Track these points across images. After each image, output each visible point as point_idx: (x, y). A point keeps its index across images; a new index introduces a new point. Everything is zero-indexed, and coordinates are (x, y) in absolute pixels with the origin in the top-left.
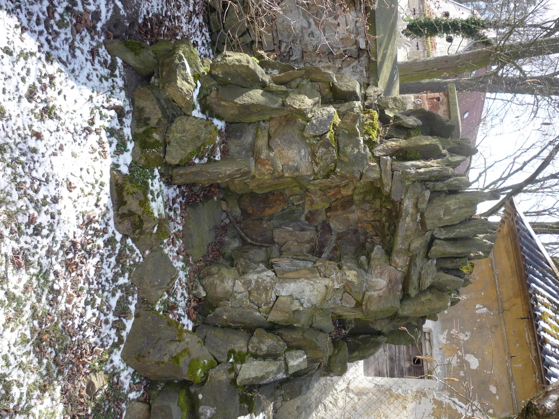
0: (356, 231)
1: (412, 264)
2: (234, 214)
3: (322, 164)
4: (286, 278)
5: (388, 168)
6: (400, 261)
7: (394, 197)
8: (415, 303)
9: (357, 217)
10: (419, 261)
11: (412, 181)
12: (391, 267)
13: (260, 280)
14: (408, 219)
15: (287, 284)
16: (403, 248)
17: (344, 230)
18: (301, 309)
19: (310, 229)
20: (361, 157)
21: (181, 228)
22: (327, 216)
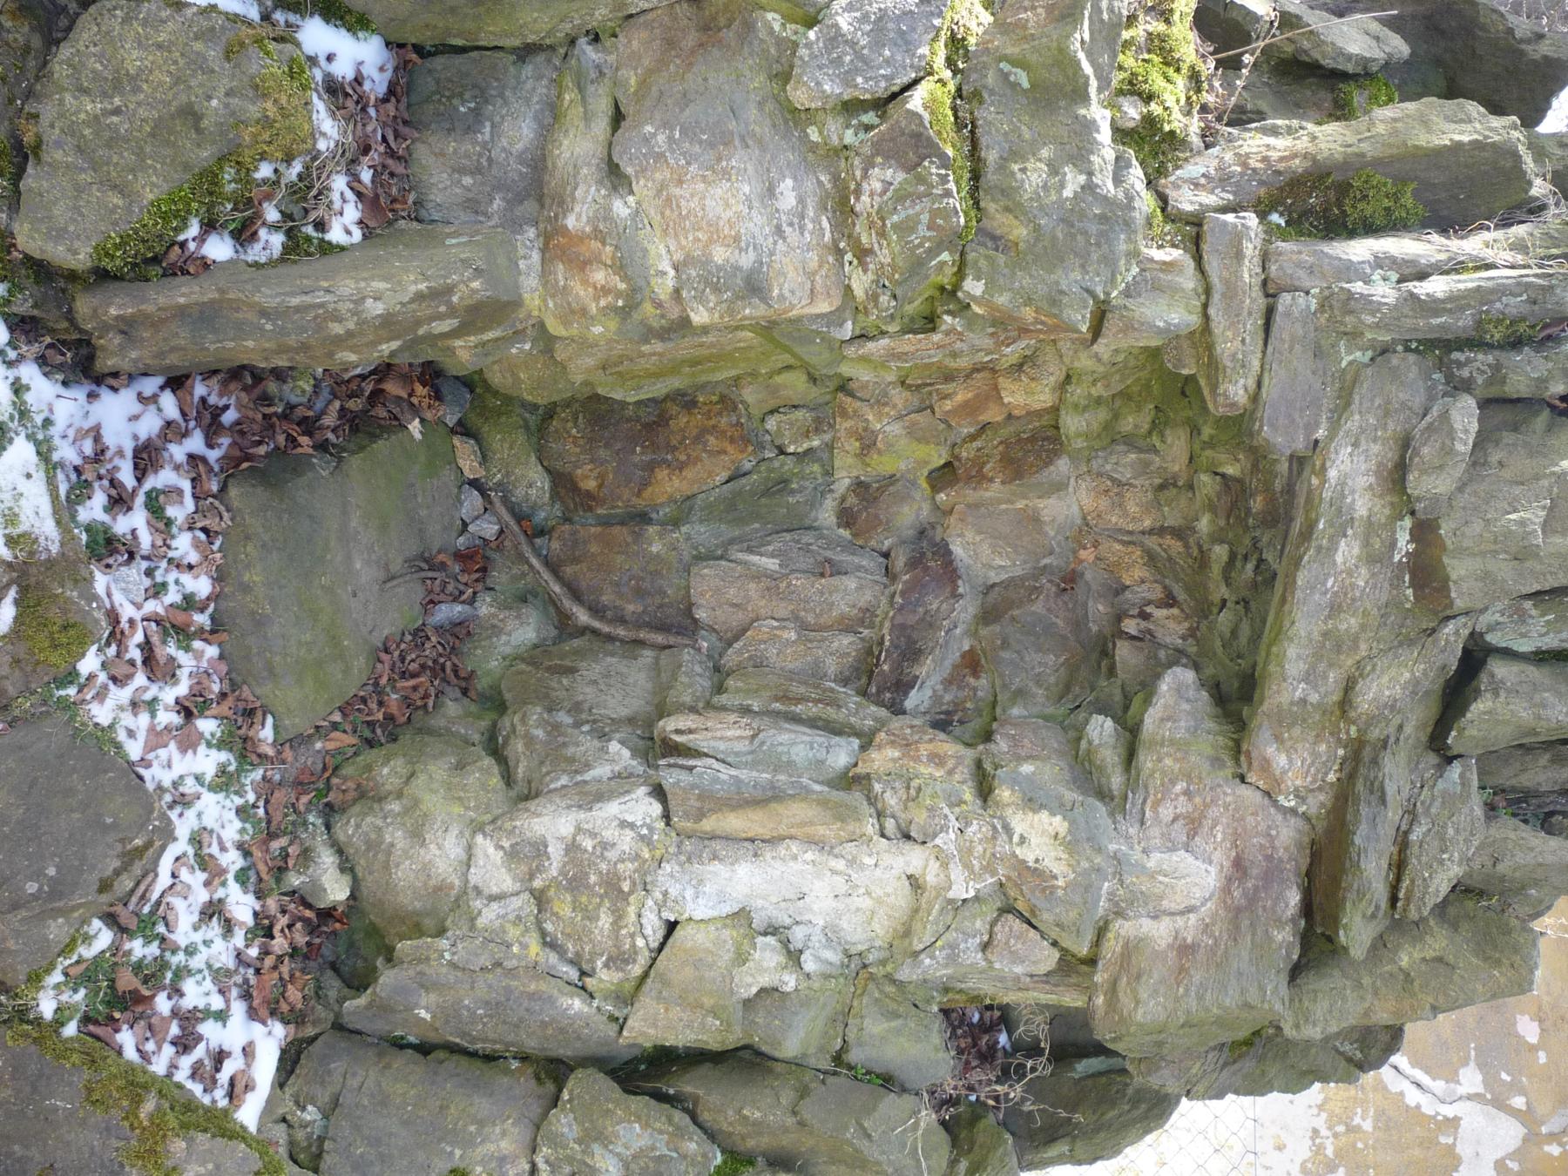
0: (1070, 580)
1: (1360, 786)
2: (519, 492)
3: (884, 256)
4: (713, 837)
5: (1249, 273)
6: (1296, 764)
7: (1280, 437)
8: (1366, 981)
9: (1075, 509)
10: (1396, 774)
11: (1372, 345)
12: (1244, 791)
13: (588, 844)
14: (1347, 552)
15: (716, 866)
16: (1314, 698)
17: (1018, 572)
18: (790, 982)
19: (859, 568)
20: (1103, 219)
21: (202, 586)
22: (936, 507)
